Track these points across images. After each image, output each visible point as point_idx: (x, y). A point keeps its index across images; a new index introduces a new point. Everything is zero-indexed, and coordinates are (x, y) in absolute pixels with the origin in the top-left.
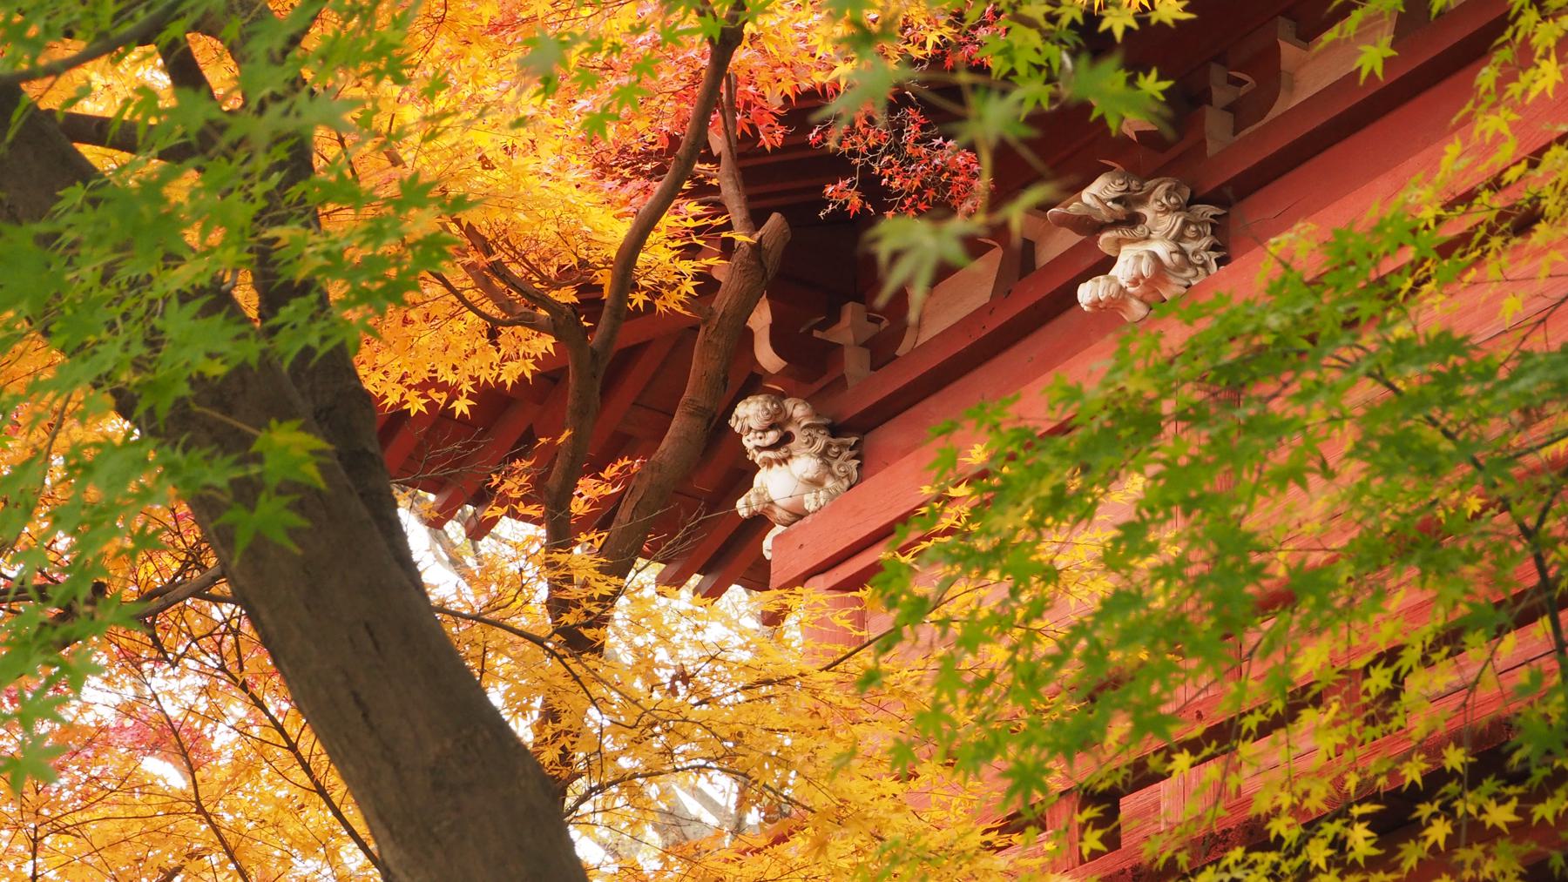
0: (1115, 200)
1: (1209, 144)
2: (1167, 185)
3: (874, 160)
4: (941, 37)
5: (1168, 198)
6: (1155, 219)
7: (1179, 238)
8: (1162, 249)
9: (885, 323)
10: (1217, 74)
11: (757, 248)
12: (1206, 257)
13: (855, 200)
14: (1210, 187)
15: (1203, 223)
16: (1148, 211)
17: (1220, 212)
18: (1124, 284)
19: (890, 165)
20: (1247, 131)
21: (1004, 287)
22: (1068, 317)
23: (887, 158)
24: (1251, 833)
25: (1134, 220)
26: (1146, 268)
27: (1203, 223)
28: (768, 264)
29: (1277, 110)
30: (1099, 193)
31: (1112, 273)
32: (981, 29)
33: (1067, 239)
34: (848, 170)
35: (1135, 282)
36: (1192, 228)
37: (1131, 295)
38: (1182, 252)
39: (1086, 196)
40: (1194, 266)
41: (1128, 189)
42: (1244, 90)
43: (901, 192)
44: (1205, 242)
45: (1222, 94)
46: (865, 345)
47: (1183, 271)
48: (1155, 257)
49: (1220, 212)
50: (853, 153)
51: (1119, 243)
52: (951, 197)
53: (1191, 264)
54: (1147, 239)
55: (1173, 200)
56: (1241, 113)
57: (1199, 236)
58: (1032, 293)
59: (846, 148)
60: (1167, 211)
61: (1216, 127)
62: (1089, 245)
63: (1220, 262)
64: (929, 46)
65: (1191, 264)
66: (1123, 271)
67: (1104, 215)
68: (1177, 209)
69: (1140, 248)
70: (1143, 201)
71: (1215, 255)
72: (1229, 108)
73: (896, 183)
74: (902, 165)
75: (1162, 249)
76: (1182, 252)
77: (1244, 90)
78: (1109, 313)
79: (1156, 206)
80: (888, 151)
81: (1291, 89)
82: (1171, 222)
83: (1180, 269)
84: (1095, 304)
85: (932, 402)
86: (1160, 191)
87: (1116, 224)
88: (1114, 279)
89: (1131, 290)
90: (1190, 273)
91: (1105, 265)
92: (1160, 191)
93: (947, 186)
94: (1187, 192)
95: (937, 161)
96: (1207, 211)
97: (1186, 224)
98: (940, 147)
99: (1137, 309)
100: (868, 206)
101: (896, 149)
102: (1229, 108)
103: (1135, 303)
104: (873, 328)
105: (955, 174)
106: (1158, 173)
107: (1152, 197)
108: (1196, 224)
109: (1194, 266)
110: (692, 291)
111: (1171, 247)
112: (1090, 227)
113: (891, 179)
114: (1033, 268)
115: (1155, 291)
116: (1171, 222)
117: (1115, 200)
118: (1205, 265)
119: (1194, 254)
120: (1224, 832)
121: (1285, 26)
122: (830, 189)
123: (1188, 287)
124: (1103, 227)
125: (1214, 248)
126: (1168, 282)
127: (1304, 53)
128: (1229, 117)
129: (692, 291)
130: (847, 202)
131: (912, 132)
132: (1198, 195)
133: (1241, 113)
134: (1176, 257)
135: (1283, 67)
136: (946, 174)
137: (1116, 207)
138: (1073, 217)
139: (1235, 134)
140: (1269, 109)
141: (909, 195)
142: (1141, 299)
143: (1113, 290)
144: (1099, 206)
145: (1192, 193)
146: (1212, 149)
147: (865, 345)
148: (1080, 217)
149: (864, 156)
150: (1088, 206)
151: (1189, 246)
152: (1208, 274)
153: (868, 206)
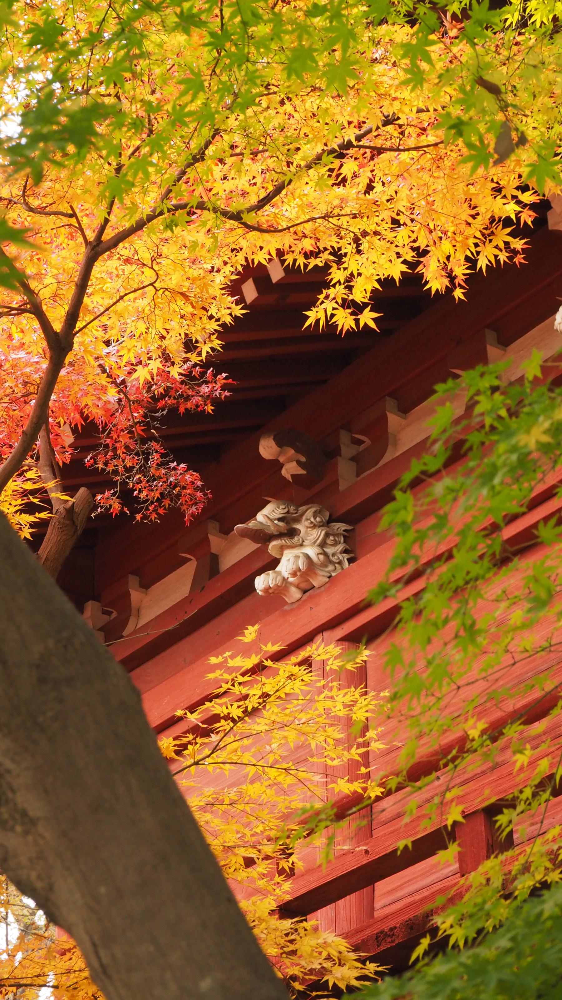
0: (279, 520)
1: (341, 483)
2: (313, 510)
3: (128, 477)
4: (212, 348)
5: (315, 518)
6: (306, 532)
7: (323, 545)
8: (312, 552)
9: (114, 615)
10: (344, 437)
11: (70, 511)
12: (341, 557)
13: (116, 506)
14: (342, 510)
15: (338, 535)
16: (301, 527)
17: (349, 527)
18: (286, 575)
19: (140, 481)
20: (366, 474)
21: (198, 584)
22: (246, 603)
23: (138, 476)
24: (411, 928)
25: (292, 533)
26: (302, 564)
27: (338, 535)
28: (78, 523)
29: (387, 457)
30: (268, 515)
31: (278, 569)
32: (204, 386)
33: (248, 547)
34: (111, 484)
35: (294, 574)
36: (332, 538)
37: (291, 584)
38: (325, 554)
39: (260, 517)
40: (333, 563)
41: (288, 512)
42: (362, 447)
43: (147, 501)
44: (340, 547)
45: (348, 450)
46: (100, 629)
47: (326, 566)
48: (307, 557)
49: (349, 527)
50: (116, 472)
51: (282, 548)
52: (181, 504)
53: (331, 562)
54: (301, 545)
55: (318, 519)
56: (361, 462)
57: (336, 544)
58: (219, 588)
59: (110, 468)
60: (314, 526)
61: (345, 473)
62: (263, 551)
63: (350, 561)
64: (204, 354)
65: (331, 562)
66: (285, 567)
67: (273, 530)
68: (321, 525)
69: (296, 551)
70: (298, 520)
71: (346, 556)
72: (353, 459)
73: (144, 493)
74: (148, 481)
75: (312, 552)
76: (325, 554)
77: (362, 447)
78: (275, 596)
79: (307, 523)
80: (139, 471)
81: (395, 445)
82: (318, 534)
83: (324, 565)
84: (267, 590)
85: (148, 666)
86: (310, 513)
87: (280, 535)
88: (279, 573)
89: (291, 579)
90: (331, 568)
91: (273, 563)
92: (310, 513)
93: (178, 496)
94: (327, 514)
95: (172, 479)
96: (341, 527)
97: (327, 535)
98: (174, 469)
99: (295, 594)
100: (126, 509)
101: (143, 470)
102: (353, 459)
103: (293, 590)
104: (106, 618)
105: (184, 488)
106: (308, 502)
107: (304, 518)
108: (334, 535)
109: (333, 563)
110: (29, 537)
111: (318, 550)
112: (263, 537)
113: (140, 491)
114: (218, 572)
115: (308, 581)
116: (318, 534)
117: (279, 520)
118: (340, 563)
119: (333, 555)
120: (391, 929)
121: (390, 403)
122: (99, 497)
123: (329, 577)
124: (271, 537)
125: (345, 551)
126: (316, 574)
127: (404, 422)
128: (354, 464)
129: (29, 537)
130: (111, 506)
131: (155, 458)
132: (334, 517)
133: (361, 462)
134: (321, 557)
135: (389, 431)
136: (178, 488)
137: (281, 524)
138: (252, 530)
139: (358, 475)
140: (382, 457)
141: (152, 503)
142: (297, 587)
143: (279, 581)
144: (269, 523)
145: (330, 516)
146: (343, 486)
147: (100, 629)
148: (257, 530)
149: (122, 475)
150: (261, 523)
151: (330, 550)
152: (342, 569)
153: (126, 509)
